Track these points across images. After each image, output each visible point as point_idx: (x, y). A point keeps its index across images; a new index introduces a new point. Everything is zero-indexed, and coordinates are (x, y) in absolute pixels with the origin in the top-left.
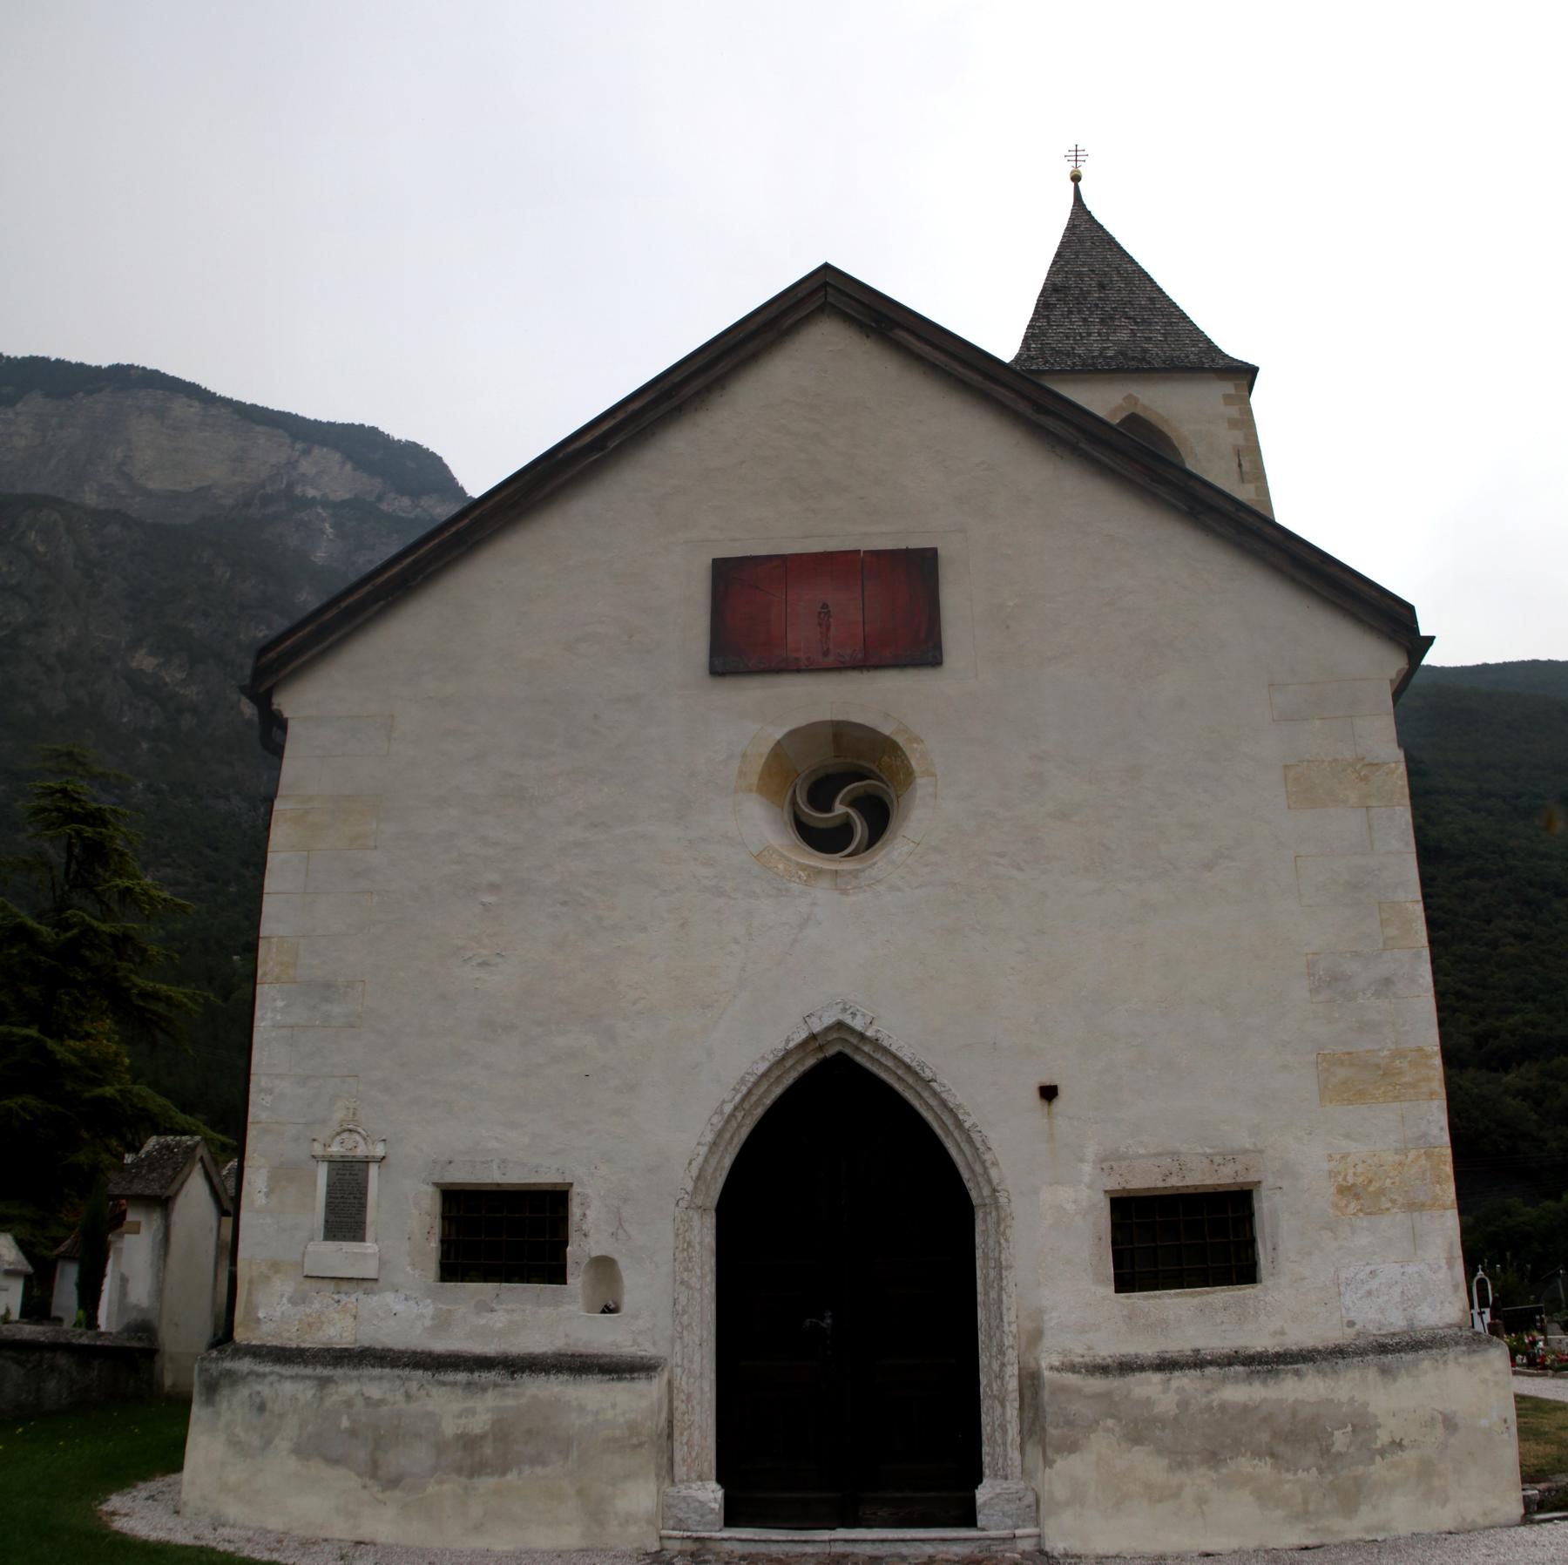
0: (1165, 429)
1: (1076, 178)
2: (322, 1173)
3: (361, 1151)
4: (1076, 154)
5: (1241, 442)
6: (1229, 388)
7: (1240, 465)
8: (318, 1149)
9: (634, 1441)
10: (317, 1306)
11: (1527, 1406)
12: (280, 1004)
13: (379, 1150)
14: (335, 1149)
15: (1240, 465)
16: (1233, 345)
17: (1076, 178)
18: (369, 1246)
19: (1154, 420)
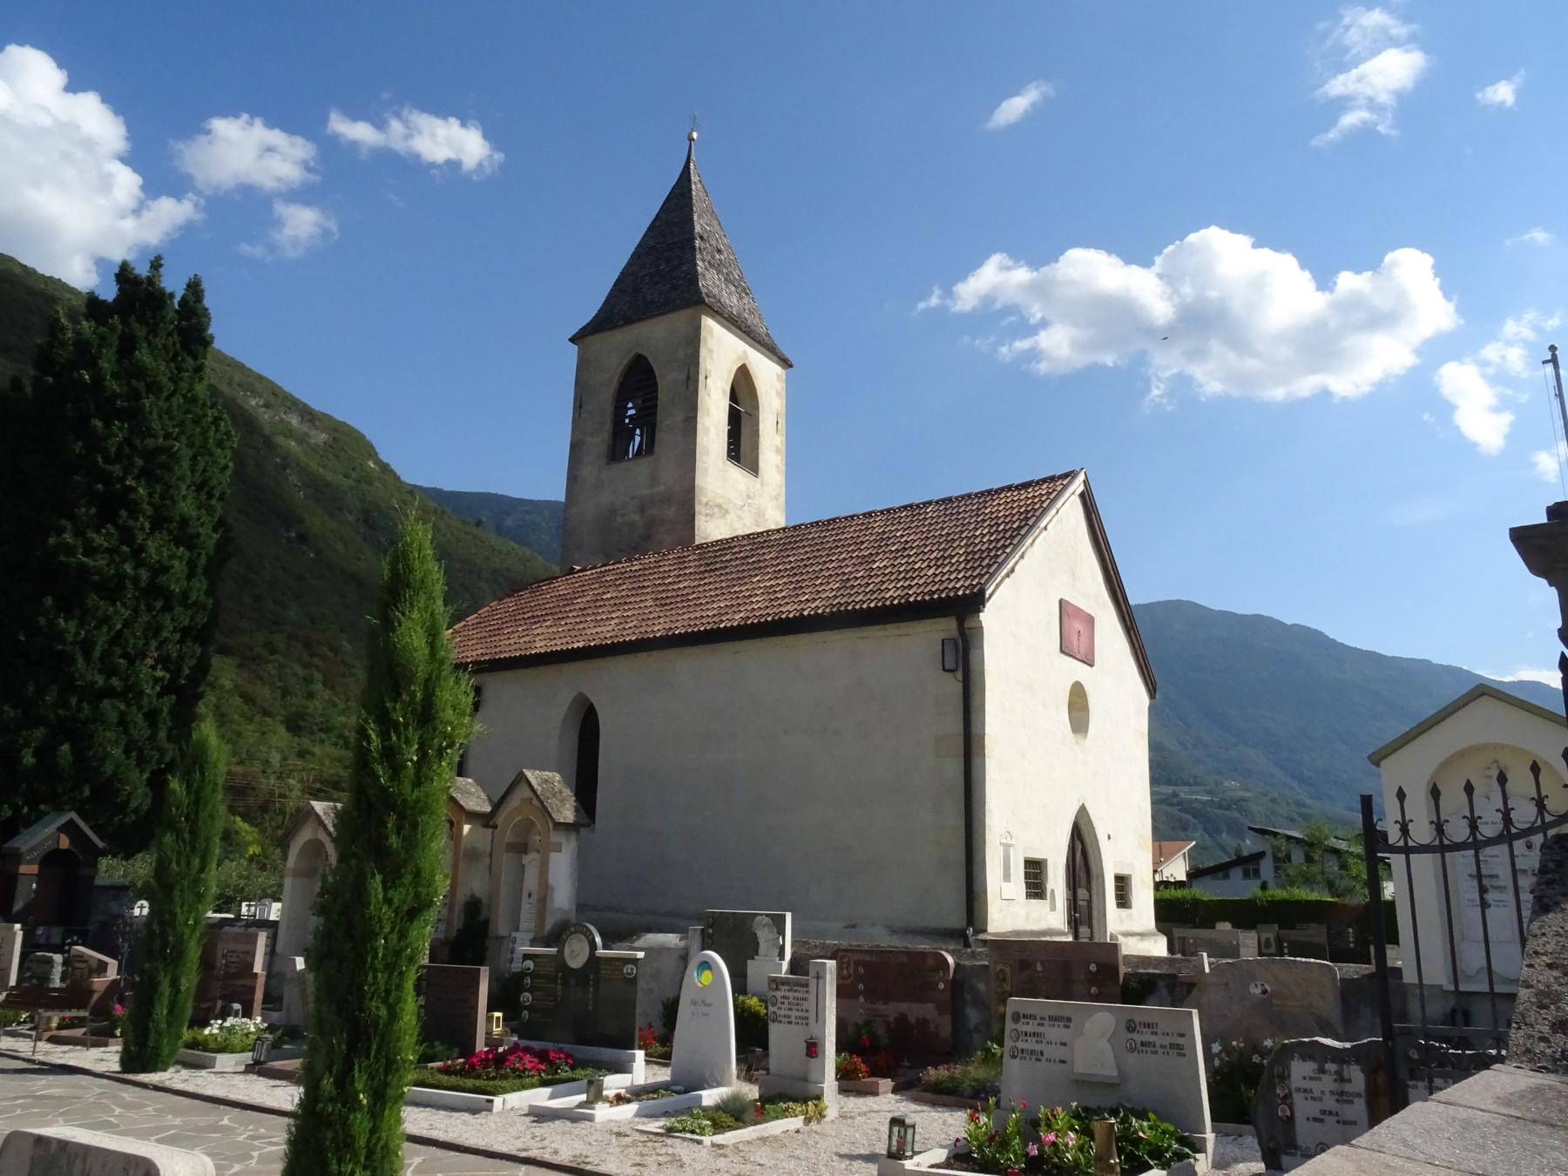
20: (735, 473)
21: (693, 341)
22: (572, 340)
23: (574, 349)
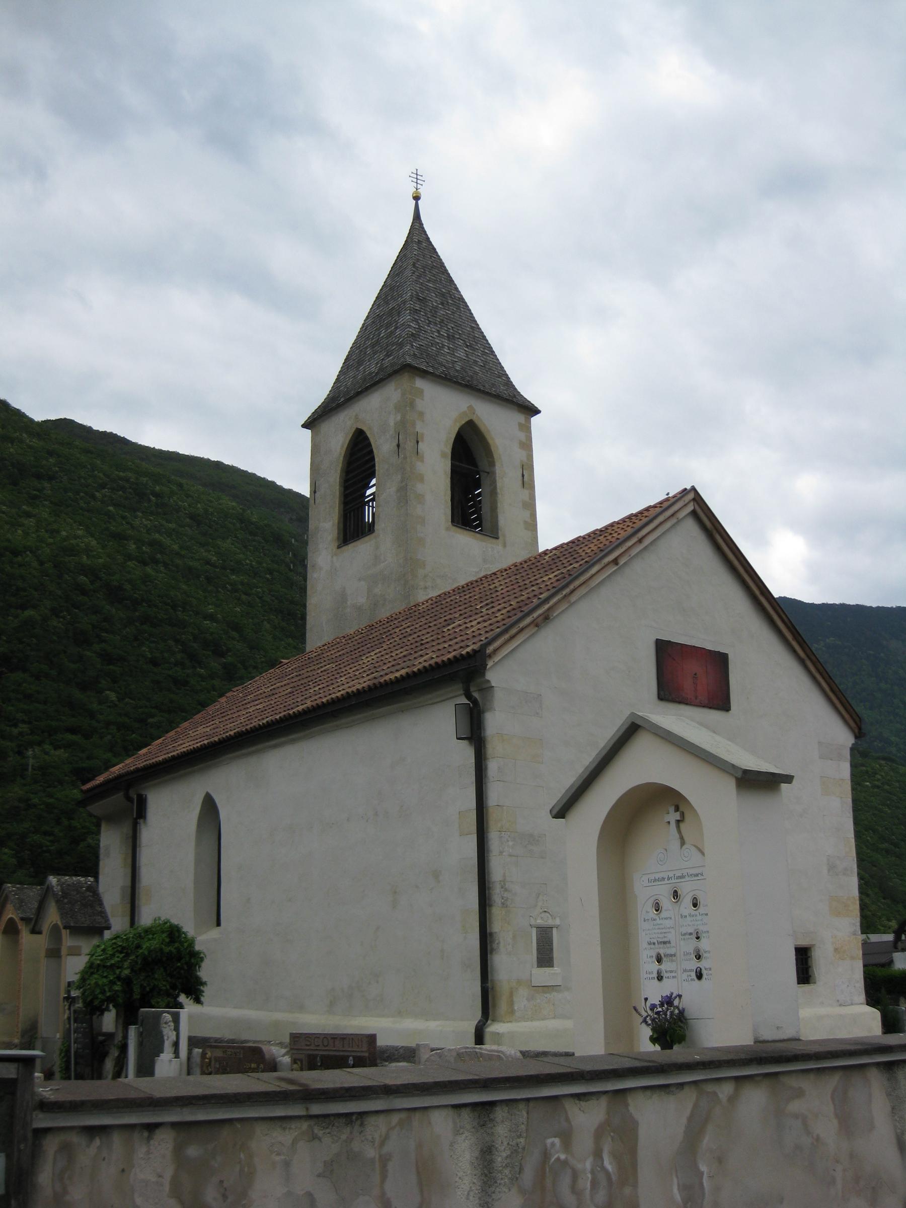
0: (487, 437)
1: (417, 198)
2: (534, 931)
3: (550, 922)
4: (417, 177)
5: (525, 459)
6: (520, 418)
7: (523, 476)
8: (533, 922)
9: (517, 1169)
10: (538, 1001)
11: (865, 944)
12: (511, 843)
13: (557, 922)
14: (539, 922)
15: (523, 476)
16: (528, 391)
17: (417, 198)
18: (556, 969)
19: (482, 429)
20: (465, 540)
21: (407, 405)
22: (305, 426)
23: (308, 432)
